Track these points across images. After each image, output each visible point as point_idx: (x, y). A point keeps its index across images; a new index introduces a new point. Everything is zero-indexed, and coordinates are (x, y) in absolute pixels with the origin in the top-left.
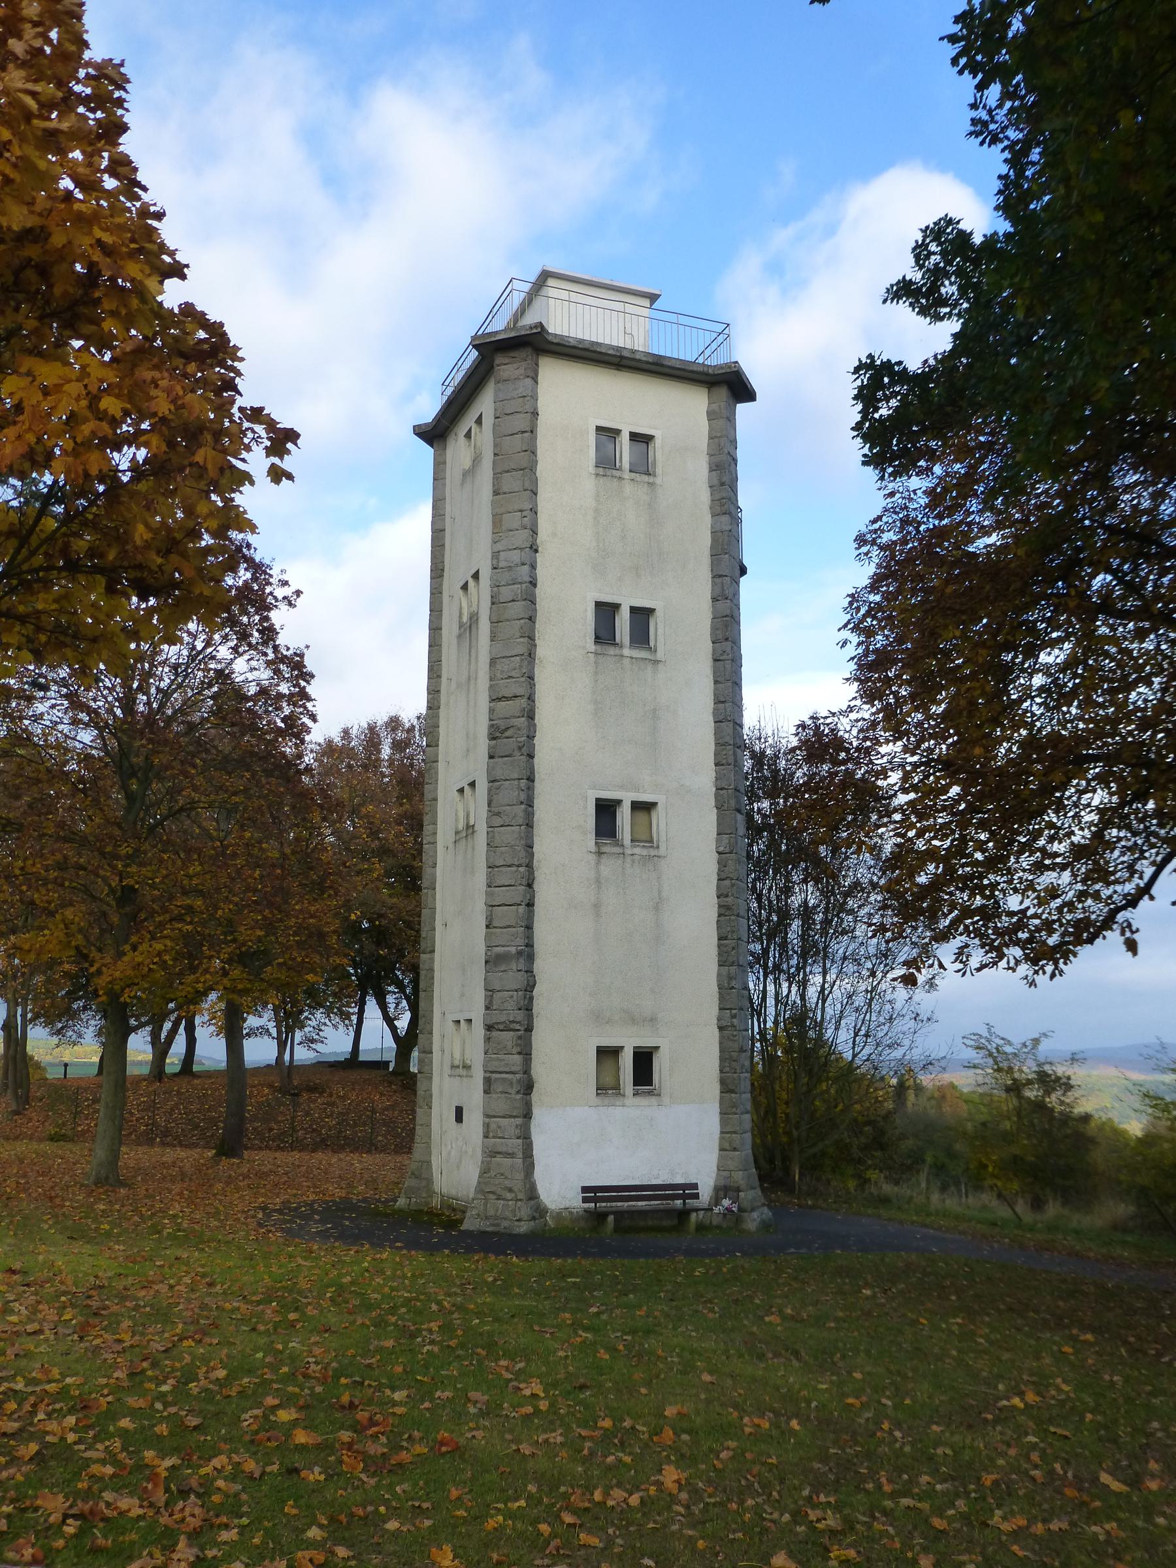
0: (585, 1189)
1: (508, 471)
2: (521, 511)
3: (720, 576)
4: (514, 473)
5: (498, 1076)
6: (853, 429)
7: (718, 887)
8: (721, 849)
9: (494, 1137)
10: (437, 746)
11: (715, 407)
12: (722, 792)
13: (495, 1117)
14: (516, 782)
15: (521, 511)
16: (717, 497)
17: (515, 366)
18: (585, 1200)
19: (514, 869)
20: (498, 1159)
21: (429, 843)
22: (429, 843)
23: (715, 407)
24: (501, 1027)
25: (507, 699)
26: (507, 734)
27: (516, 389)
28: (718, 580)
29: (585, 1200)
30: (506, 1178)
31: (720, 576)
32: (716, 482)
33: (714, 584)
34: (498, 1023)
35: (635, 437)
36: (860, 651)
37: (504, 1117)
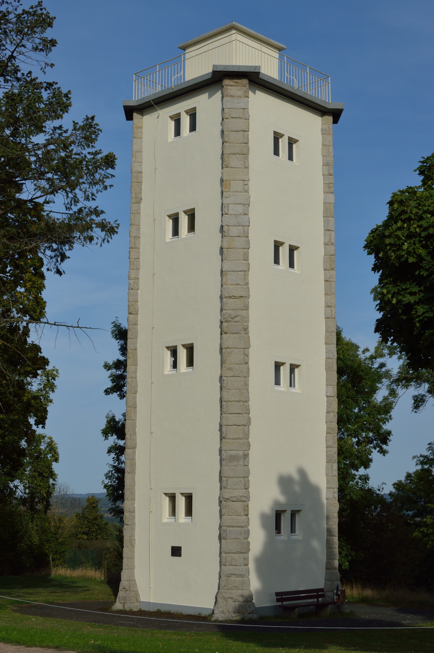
0: (277, 594)
1: (234, 154)
2: (243, 180)
3: (329, 230)
4: (238, 156)
5: (231, 529)
6: (55, 46)
7: (327, 417)
8: (329, 394)
9: (229, 565)
10: (137, 314)
11: (326, 126)
12: (329, 360)
13: (229, 553)
14: (242, 350)
15: (243, 180)
16: (327, 182)
17: (239, 88)
18: (278, 600)
19: (241, 403)
20: (233, 578)
21: (132, 378)
22: (132, 378)
23: (326, 126)
24: (234, 499)
25: (235, 297)
26: (236, 319)
27: (238, 103)
28: (328, 233)
29: (278, 600)
30: (239, 589)
31: (329, 230)
32: (326, 173)
33: (325, 235)
34: (231, 497)
35: (290, 139)
36: (73, 213)
37: (235, 553)
